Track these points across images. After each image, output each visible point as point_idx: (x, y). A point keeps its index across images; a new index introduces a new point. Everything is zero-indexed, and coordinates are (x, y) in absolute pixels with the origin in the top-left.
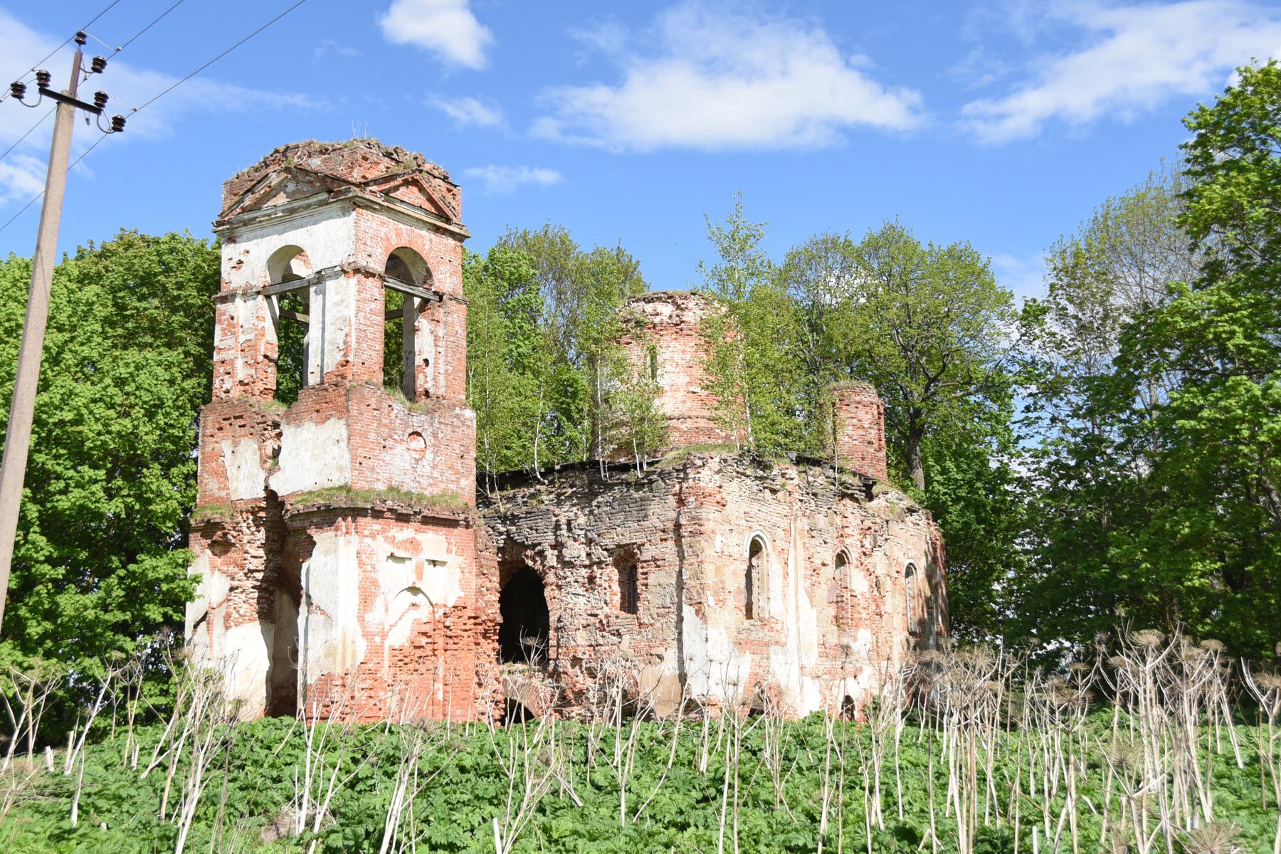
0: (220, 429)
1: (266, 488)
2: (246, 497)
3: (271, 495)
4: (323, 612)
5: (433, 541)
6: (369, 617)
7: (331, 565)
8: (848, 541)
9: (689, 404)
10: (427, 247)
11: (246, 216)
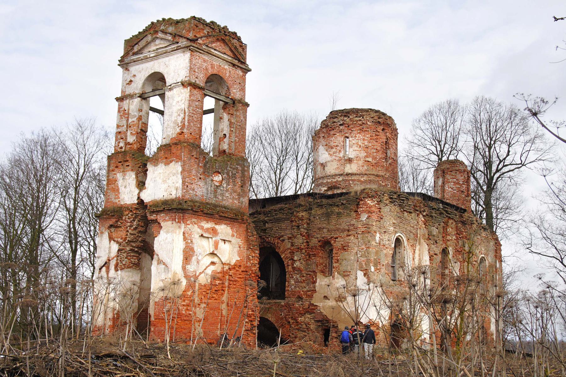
0: (117, 167)
1: (139, 198)
2: (128, 203)
3: (141, 202)
4: (164, 264)
5: (224, 229)
6: (188, 267)
7: (169, 240)
8: (449, 243)
9: (365, 167)
10: (227, 75)
11: (135, 57)
